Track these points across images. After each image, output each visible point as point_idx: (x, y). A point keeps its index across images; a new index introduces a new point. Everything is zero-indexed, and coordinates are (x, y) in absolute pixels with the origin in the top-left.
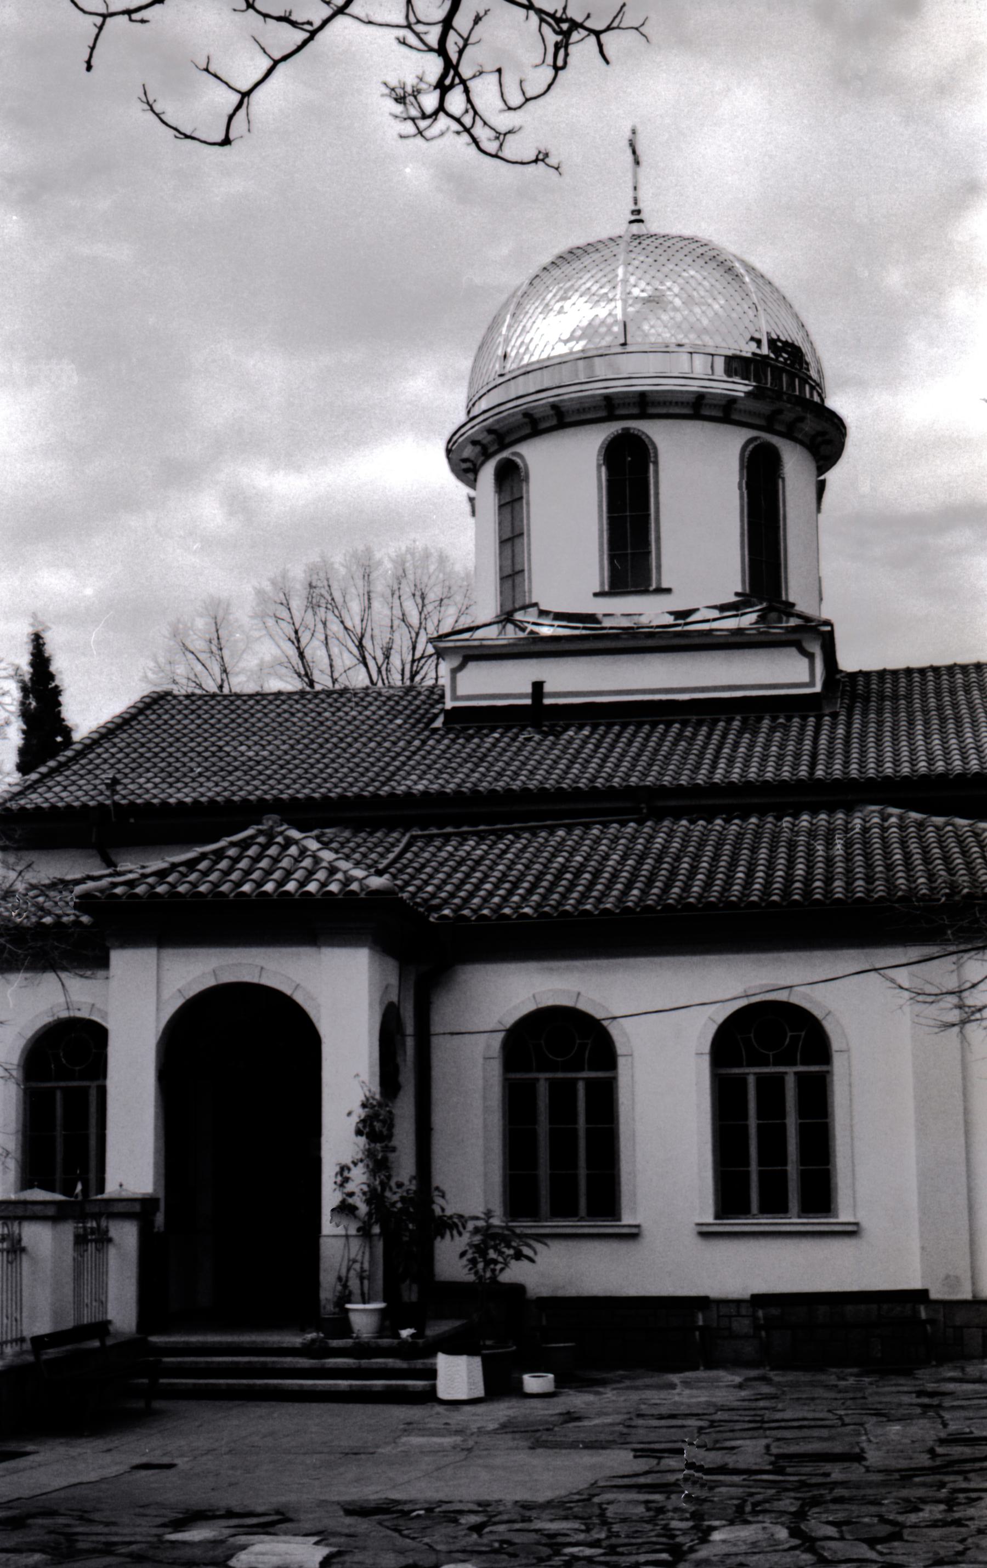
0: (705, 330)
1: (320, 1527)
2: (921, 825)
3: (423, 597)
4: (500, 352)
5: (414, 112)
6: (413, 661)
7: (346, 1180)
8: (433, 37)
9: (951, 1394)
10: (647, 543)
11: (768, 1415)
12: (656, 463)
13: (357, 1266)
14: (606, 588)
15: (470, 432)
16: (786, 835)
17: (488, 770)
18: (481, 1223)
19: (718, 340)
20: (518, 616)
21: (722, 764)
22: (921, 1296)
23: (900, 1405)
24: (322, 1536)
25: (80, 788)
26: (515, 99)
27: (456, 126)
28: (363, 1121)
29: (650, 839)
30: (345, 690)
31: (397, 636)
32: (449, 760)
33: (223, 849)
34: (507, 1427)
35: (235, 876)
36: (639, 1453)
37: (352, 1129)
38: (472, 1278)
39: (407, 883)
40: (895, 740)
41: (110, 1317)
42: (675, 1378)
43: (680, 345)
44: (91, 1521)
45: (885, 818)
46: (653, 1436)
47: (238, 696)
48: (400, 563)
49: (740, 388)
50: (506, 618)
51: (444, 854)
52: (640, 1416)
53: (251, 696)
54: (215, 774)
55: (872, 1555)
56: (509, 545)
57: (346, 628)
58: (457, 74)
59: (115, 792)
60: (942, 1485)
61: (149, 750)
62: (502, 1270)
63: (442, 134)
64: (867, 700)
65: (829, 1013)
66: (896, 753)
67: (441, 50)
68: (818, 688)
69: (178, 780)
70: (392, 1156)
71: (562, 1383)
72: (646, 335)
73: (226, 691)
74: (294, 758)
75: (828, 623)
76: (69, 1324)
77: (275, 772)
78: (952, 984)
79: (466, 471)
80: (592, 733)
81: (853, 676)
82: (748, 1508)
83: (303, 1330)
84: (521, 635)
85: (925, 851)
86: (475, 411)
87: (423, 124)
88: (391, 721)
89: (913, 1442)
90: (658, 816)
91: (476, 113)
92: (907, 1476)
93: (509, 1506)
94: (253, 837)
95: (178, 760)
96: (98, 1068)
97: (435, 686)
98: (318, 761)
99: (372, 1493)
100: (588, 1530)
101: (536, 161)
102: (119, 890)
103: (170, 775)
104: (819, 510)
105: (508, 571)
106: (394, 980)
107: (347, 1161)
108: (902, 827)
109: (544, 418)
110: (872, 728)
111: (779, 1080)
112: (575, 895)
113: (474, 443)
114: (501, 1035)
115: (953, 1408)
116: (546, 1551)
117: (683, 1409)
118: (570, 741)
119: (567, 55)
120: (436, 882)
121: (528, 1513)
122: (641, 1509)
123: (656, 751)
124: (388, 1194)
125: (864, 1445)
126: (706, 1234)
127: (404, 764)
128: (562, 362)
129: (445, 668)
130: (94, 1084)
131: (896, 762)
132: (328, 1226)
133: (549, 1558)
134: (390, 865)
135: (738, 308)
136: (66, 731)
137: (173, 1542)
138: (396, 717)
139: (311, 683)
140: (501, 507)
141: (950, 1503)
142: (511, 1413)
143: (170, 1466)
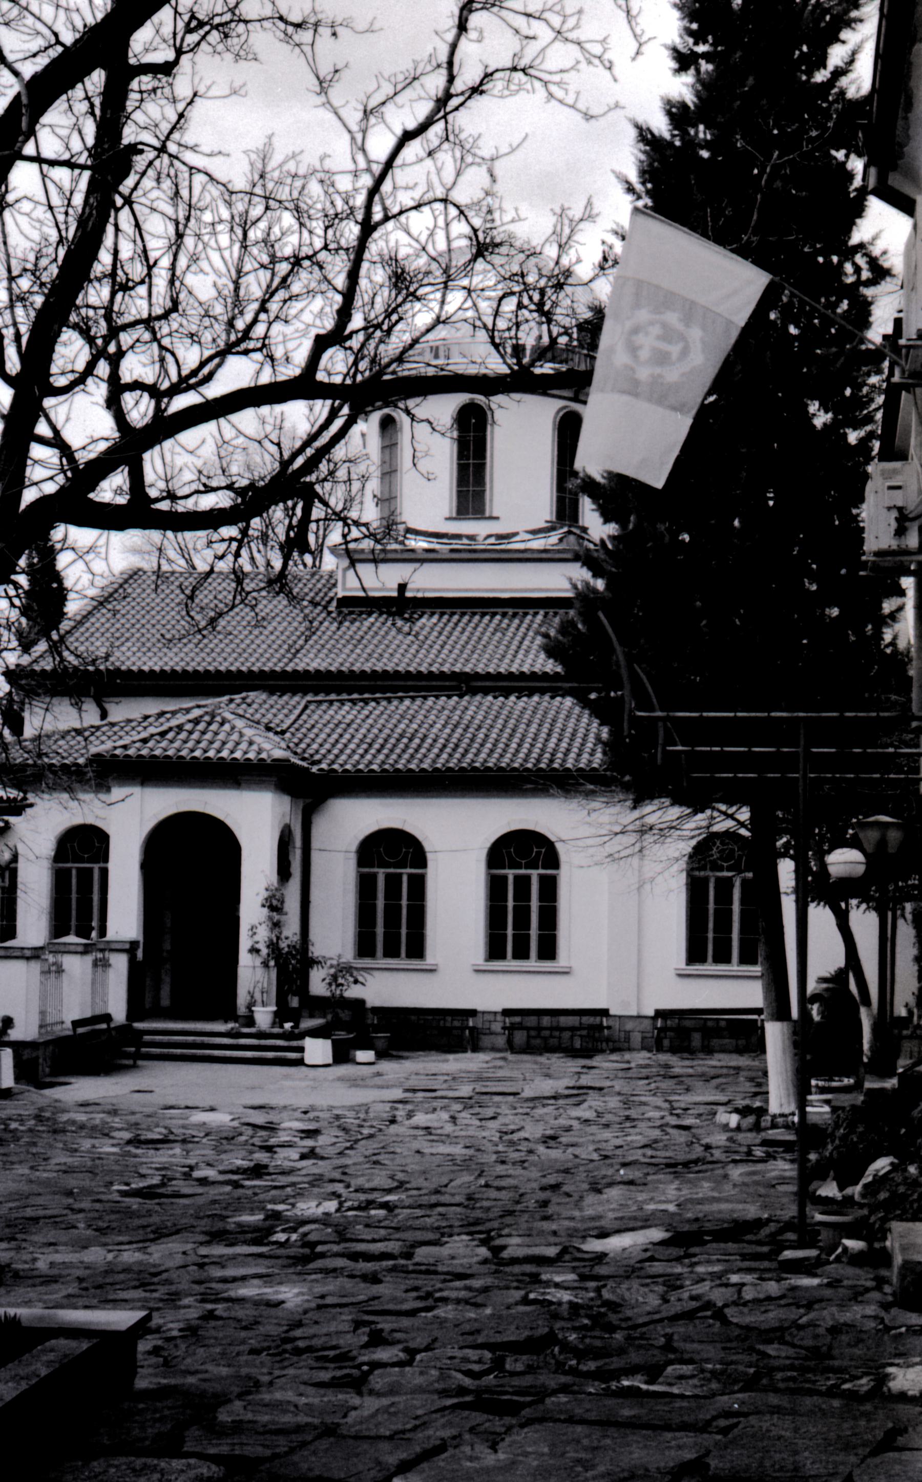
13: (260, 985)
14: (454, 515)
28: (266, 899)
32: (337, 641)
34: (340, 1079)
37: (259, 904)
38: (328, 994)
56: (388, 477)
71: (382, 1055)
76: (88, 1014)
80: (439, 620)
83: (226, 1022)
90: (474, 692)
96: (104, 856)
102: (118, 752)
107: (256, 922)
111: (528, 878)
130: (96, 867)
132: (245, 958)
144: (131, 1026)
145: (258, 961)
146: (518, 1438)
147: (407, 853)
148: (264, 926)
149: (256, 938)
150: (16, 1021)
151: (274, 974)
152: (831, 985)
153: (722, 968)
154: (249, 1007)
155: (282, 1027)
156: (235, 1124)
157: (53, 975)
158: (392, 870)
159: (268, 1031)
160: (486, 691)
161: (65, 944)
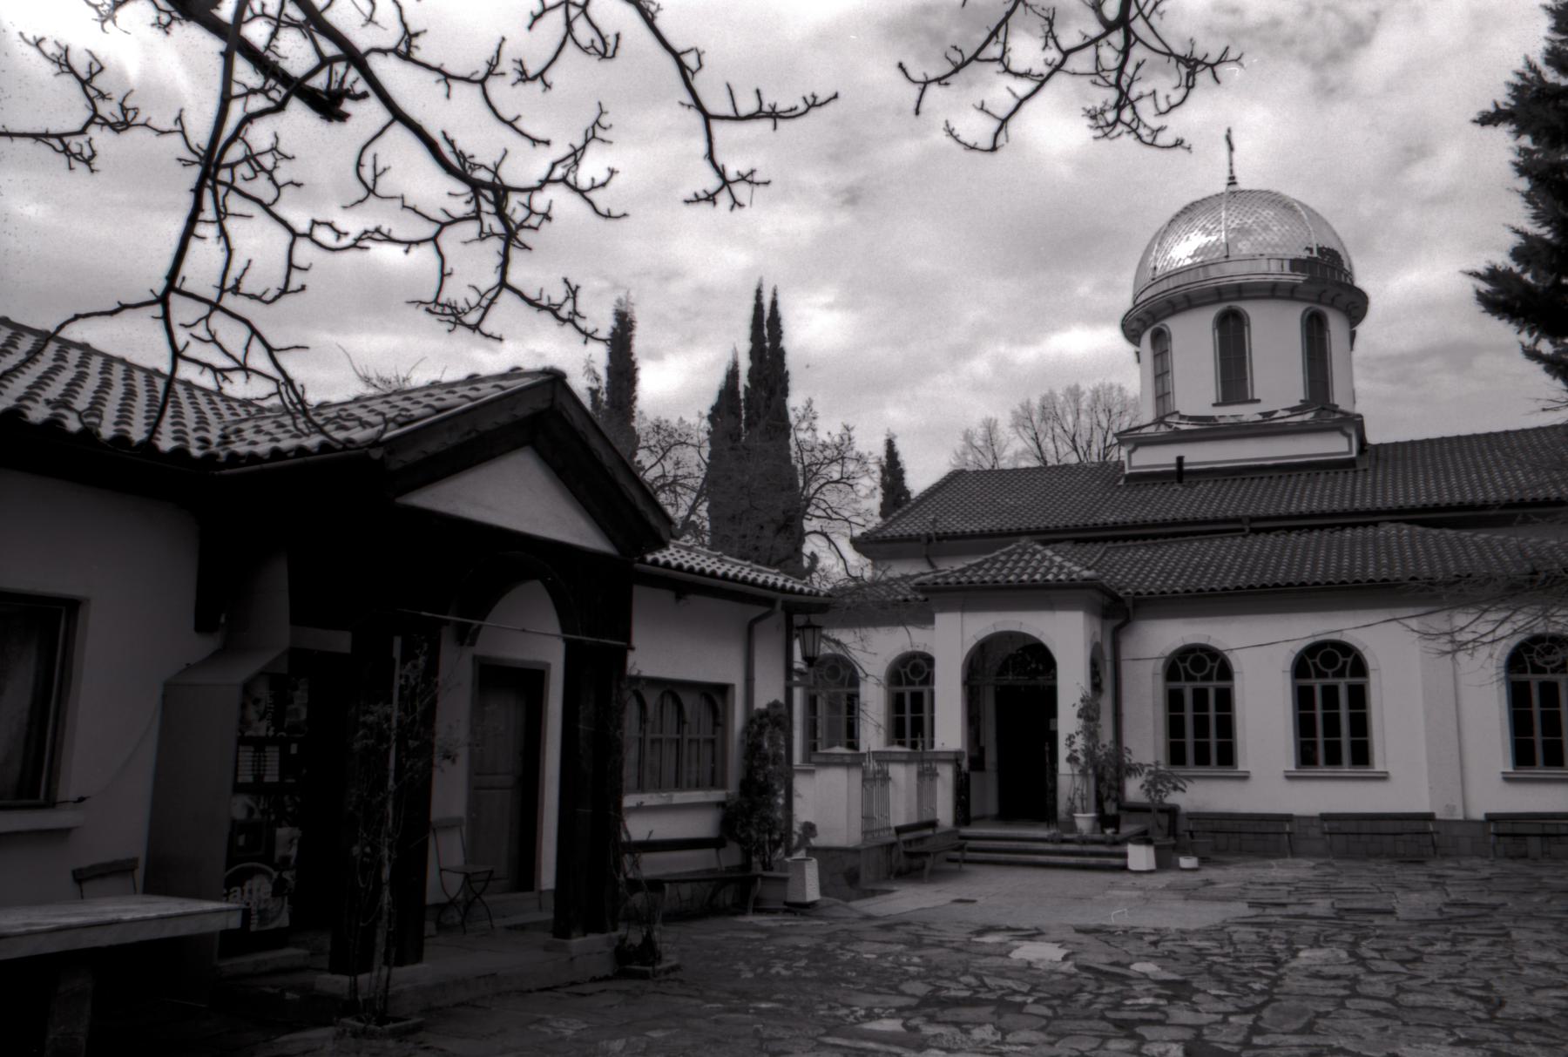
0: (1277, 245)
1: (1061, 939)
2: (1423, 535)
3: (1110, 411)
4: (1152, 266)
5: (1102, 123)
6: (1105, 448)
7: (1073, 743)
8: (1112, 78)
9: (1451, 876)
10: (1244, 373)
11: (1332, 885)
12: (1249, 325)
13: (1079, 792)
14: (1220, 401)
15: (1135, 314)
17: (1152, 508)
18: (1153, 769)
19: (1285, 250)
21: (1295, 501)
22: (1429, 817)
23: (1417, 882)
24: (1062, 943)
25: (916, 525)
27: (1126, 129)
29: (1251, 546)
30: (1066, 465)
31: (1095, 434)
33: (997, 556)
35: (1005, 571)
36: (1252, 905)
39: (1105, 574)
40: (1395, 487)
41: (938, 817)
42: (1273, 862)
43: (1261, 255)
44: (930, 929)
45: (1399, 531)
46: (1259, 895)
47: (1003, 471)
48: (1096, 392)
49: (1300, 278)
50: (1159, 421)
51: (1127, 557)
52: (1251, 883)
53: (1011, 471)
54: (991, 515)
55: (1402, 970)
57: (1065, 431)
58: (1127, 98)
59: (935, 527)
60: (1448, 931)
61: (954, 502)
62: (1166, 796)
63: (1119, 135)
64: (1386, 461)
65: (1284, 672)
66: (1417, 489)
67: (1118, 85)
68: (1354, 455)
69: (971, 519)
70: (1099, 730)
71: (1204, 861)
72: (1241, 250)
73: (996, 468)
74: (1037, 505)
75: (1360, 416)
76: (914, 820)
77: (1026, 513)
78: (1446, 628)
79: (1134, 336)
81: (1377, 447)
82: (1322, 938)
84: (1169, 430)
85: (1427, 550)
86: (1138, 301)
87: (1107, 130)
88: (1093, 482)
89: (1427, 904)
91: (1139, 120)
92: (1424, 924)
93: (1173, 931)
94: (1014, 549)
95: (970, 507)
96: (929, 679)
97: (1119, 461)
98: (1051, 506)
99: (1091, 921)
100: (1222, 947)
101: (1175, 145)
102: (939, 580)
103: (966, 516)
104: (1352, 349)
105: (1160, 393)
106: (1098, 629)
107: (1073, 732)
110: (1390, 477)
112: (1206, 579)
113: (1139, 320)
114: (1161, 662)
115: (1453, 885)
116: (1196, 958)
117: (1279, 880)
119: (1194, 80)
120: (1122, 573)
121: (1184, 936)
122: (1254, 937)
124: (1097, 751)
125: (1395, 905)
126: (1290, 777)
127: (1101, 506)
128: (1189, 269)
129: (1124, 452)
131: (1406, 496)
132: (1064, 767)
133: (1198, 962)
134: (1096, 563)
135: (1298, 231)
136: (907, 493)
137: (976, 942)
138: (1096, 480)
139: (1045, 463)
141: (1454, 942)
142: (1172, 879)
143: (973, 901)
147: (1212, 668)
148: (1081, 736)
149: (1074, 747)
151: (1092, 782)
154: (1072, 811)
155: (1103, 832)
156: (1068, 967)
157: (879, 783)
158: (1199, 684)
159: (1091, 836)
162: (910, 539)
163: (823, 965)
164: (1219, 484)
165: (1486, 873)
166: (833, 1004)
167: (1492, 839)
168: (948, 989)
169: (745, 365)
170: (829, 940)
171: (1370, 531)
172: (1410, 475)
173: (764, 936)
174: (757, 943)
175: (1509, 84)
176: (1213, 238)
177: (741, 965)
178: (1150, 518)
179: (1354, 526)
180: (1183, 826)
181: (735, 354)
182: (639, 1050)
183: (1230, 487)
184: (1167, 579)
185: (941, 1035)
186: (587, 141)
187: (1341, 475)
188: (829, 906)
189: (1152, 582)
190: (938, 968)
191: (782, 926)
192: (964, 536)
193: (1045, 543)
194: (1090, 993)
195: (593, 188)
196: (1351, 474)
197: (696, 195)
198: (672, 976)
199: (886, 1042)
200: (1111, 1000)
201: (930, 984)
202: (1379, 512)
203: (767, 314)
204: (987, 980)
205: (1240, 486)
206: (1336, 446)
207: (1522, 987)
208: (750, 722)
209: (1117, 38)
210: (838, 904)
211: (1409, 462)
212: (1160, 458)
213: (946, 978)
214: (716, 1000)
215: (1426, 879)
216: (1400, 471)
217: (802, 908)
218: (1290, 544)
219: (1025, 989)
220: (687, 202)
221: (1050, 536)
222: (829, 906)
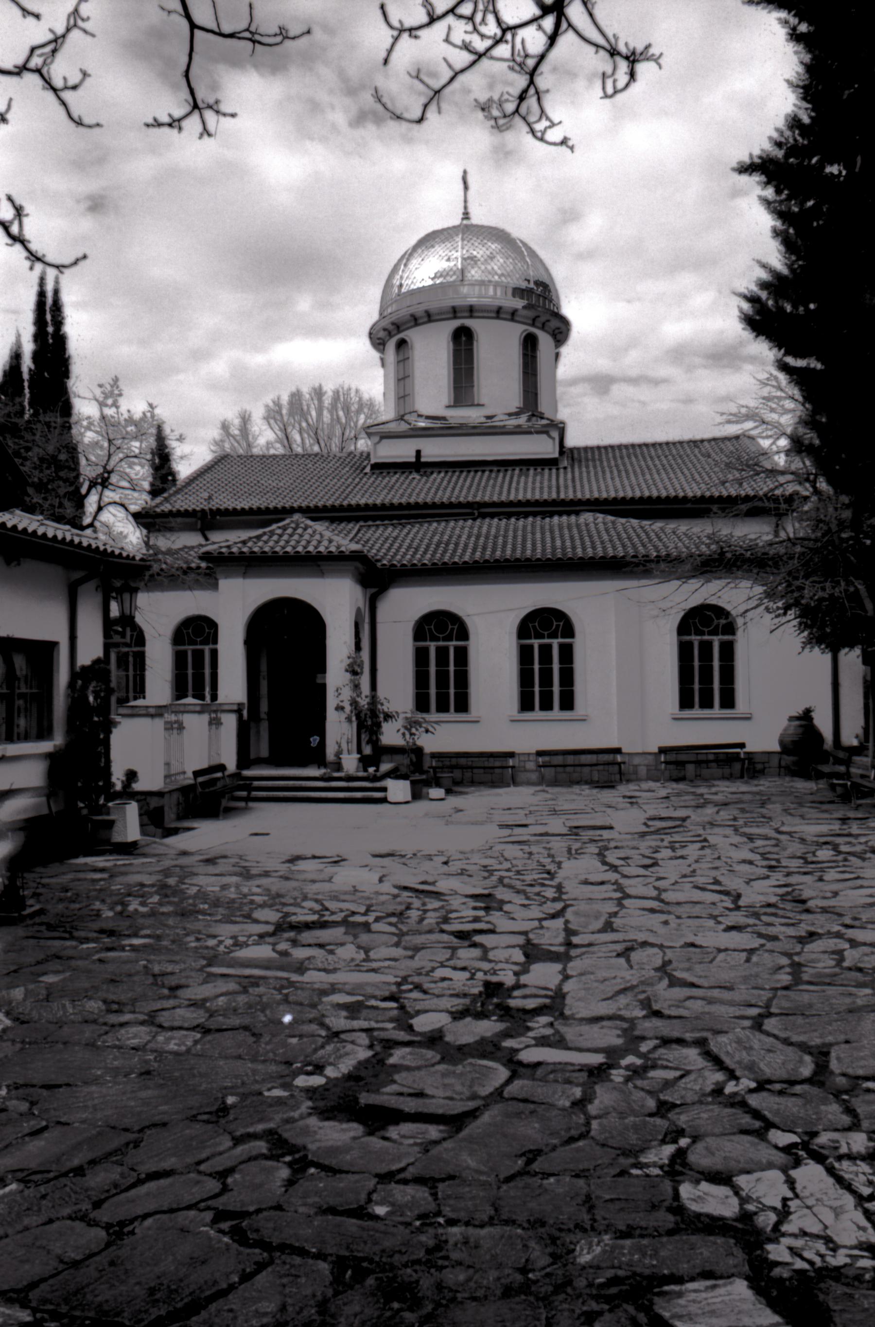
16: (565, 525)
20: (406, 418)
21: (480, 493)
26: (610, 90)
29: (480, 527)
40: (597, 481)
48: (336, 393)
50: (401, 418)
64: (580, 461)
71: (449, 792)
75: (563, 423)
76: (205, 765)
79: (379, 344)
85: (618, 534)
90: (483, 516)
102: (224, 550)
105: (402, 394)
107: (340, 684)
108: (605, 523)
109: (421, 317)
113: (385, 330)
116: (486, 874)
118: (435, 480)
123: (479, 484)
130: (207, 649)
132: (331, 715)
140: (398, 362)
141: (673, 849)
144: (240, 774)
145: (343, 716)
146: (719, 1241)
147: (452, 629)
150: (140, 775)
151: (355, 724)
152: (803, 723)
153: (707, 712)
154: (338, 754)
157: (175, 731)
158: (441, 643)
160: (492, 516)
161: (185, 705)
162: (186, 514)
163: (176, 900)
164: (450, 474)
165: (663, 793)
166: (200, 936)
167: (663, 766)
168: (295, 914)
169: (28, 348)
170: (167, 876)
171: (573, 518)
172: (600, 474)
173: (105, 875)
174: (102, 883)
175: (770, 138)
176: (452, 264)
177: (97, 905)
178: (395, 501)
179: (560, 514)
180: (427, 763)
181: (18, 336)
182: (41, 997)
183: (459, 477)
184: (415, 553)
185: (314, 957)
186: (68, 30)
187: (546, 471)
188: (147, 845)
189: (404, 557)
190: (279, 895)
191: (115, 865)
192: (235, 512)
193: (314, 519)
194: (418, 909)
195: (66, 88)
196: (554, 471)
197: (155, 120)
198: (37, 920)
199: (267, 968)
200: (437, 914)
201: (278, 910)
202: (580, 502)
203: (49, 300)
204: (327, 904)
205: (467, 477)
206: (544, 447)
207: (741, 880)
208: (75, 675)
209: (548, 23)
210: (155, 843)
211: (598, 463)
212: (403, 451)
213: (291, 905)
214: (87, 940)
215: (621, 799)
216: (591, 469)
217: (129, 849)
218: (512, 527)
219: (362, 909)
220: (148, 125)
221: (316, 513)
222: (147, 845)
